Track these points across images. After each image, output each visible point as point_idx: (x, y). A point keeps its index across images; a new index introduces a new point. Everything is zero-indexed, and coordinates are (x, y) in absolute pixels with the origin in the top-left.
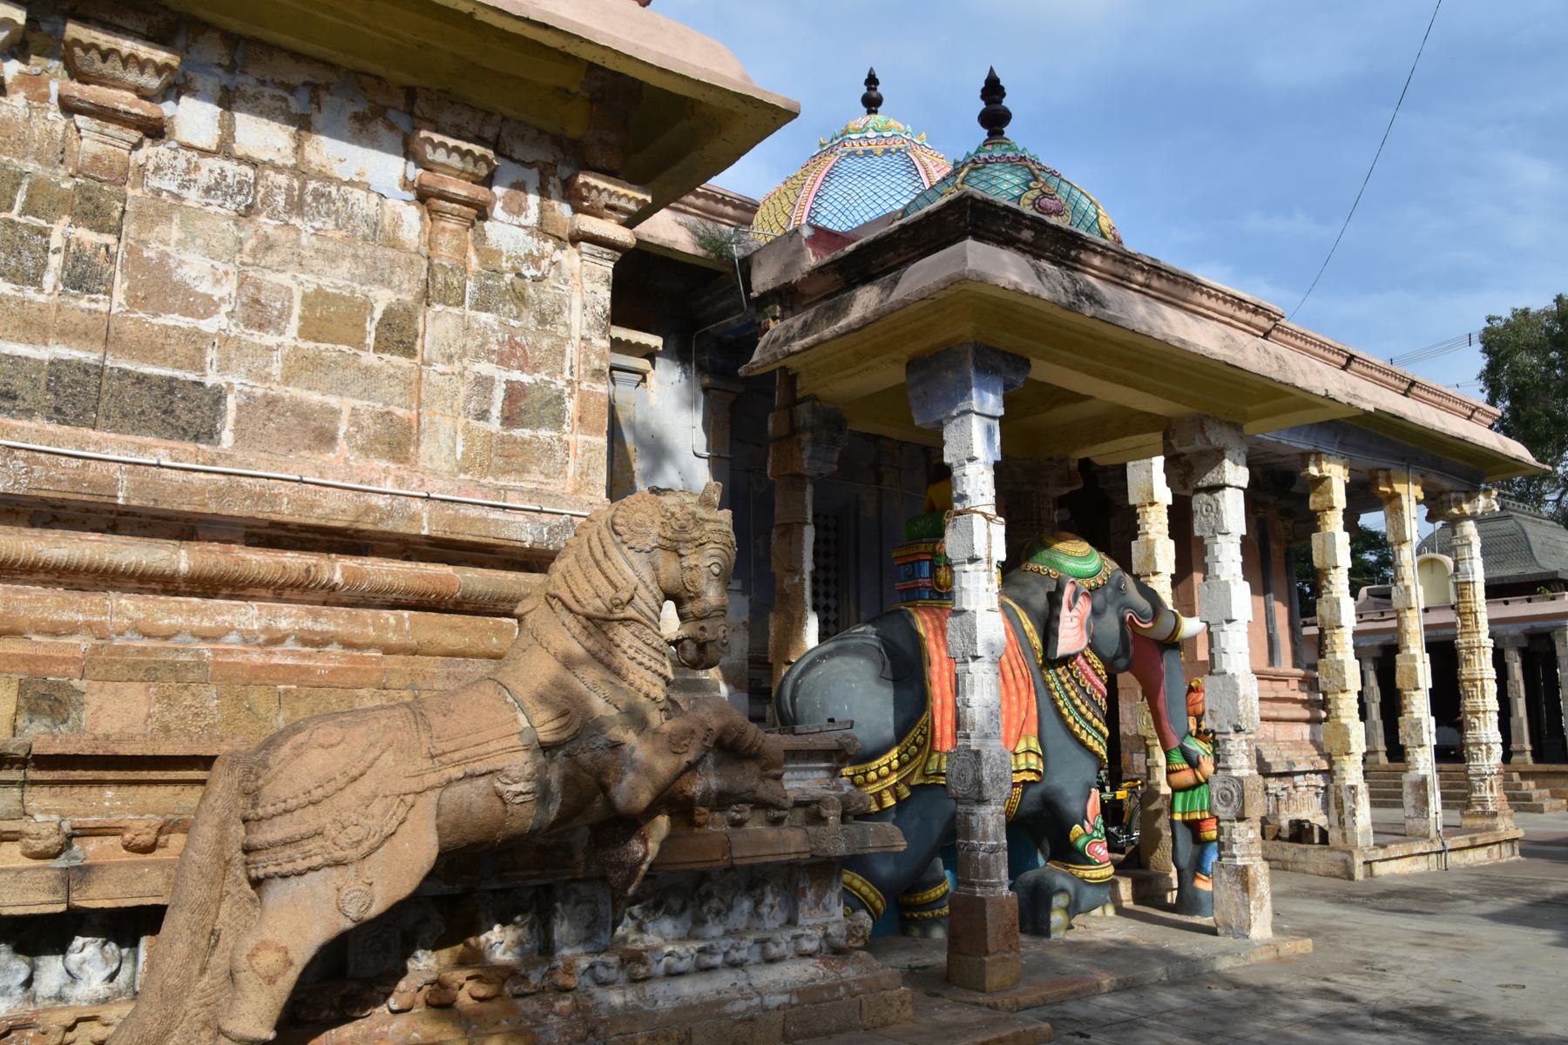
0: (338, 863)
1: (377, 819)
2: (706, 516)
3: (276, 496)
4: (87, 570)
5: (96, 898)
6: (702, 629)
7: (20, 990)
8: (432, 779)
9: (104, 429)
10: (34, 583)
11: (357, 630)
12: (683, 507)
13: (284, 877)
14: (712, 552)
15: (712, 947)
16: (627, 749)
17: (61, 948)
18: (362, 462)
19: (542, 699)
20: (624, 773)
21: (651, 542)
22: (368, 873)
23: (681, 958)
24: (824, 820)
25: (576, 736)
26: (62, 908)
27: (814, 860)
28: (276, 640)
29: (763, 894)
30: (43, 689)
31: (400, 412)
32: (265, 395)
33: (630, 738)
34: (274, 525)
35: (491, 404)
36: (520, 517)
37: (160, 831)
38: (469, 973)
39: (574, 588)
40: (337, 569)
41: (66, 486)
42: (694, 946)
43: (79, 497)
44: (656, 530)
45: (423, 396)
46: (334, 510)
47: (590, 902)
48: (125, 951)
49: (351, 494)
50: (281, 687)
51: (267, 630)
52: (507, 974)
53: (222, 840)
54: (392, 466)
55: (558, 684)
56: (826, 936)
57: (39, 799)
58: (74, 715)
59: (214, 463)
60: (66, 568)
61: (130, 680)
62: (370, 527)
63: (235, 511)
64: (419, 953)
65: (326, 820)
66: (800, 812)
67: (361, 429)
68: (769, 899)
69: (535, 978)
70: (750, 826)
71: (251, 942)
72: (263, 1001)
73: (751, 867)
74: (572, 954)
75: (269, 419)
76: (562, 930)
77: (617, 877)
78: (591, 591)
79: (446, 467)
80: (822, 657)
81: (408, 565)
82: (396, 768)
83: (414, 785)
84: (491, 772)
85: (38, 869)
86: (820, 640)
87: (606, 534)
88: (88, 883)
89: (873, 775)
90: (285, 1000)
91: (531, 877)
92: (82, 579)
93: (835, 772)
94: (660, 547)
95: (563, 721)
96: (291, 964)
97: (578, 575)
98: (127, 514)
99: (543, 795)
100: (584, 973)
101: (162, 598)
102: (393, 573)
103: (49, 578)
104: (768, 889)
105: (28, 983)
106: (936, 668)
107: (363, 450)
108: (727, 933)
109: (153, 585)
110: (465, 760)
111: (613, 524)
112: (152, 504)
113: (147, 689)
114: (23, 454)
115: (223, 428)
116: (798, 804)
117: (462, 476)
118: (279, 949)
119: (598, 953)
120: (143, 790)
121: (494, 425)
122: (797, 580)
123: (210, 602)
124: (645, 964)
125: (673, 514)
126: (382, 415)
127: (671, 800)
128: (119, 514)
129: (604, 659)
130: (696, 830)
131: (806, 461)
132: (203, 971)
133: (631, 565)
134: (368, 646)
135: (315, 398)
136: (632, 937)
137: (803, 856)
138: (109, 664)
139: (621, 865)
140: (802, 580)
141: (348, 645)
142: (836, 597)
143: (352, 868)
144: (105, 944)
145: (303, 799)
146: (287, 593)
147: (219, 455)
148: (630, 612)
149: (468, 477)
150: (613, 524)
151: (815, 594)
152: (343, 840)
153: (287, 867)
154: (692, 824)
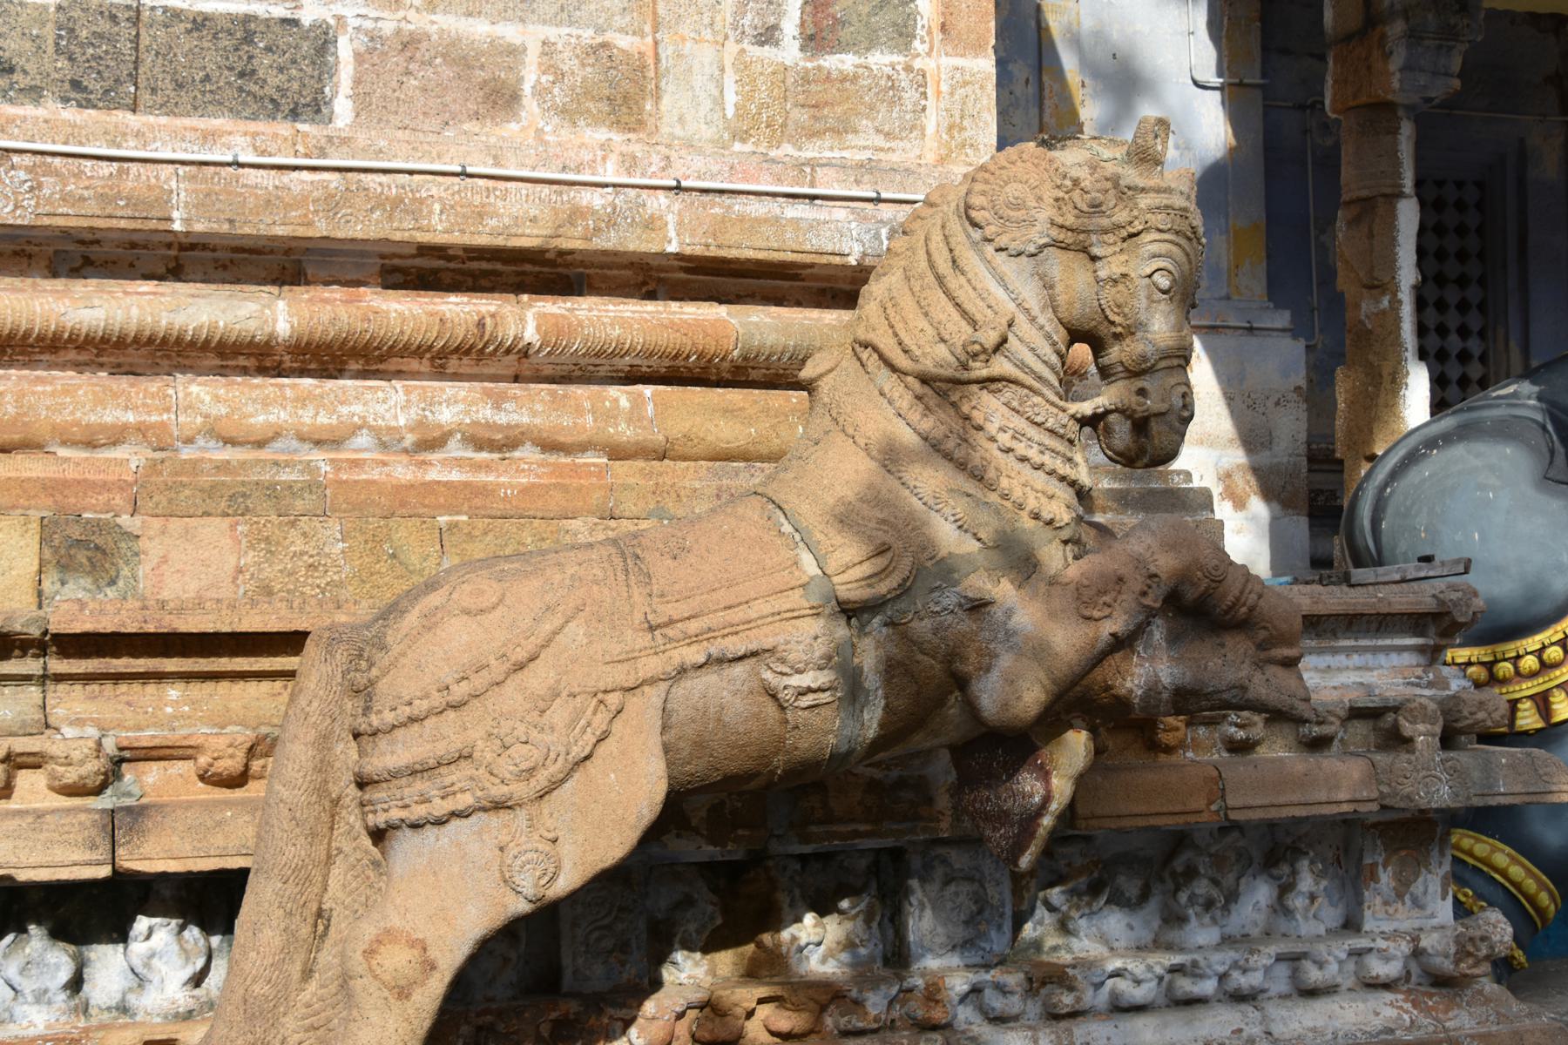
0: (498, 806)
1: (560, 733)
2: (1141, 183)
3: (422, 201)
4: (136, 340)
5: (153, 855)
6: (1142, 392)
7: (63, 996)
8: (651, 665)
9: (150, 109)
10: (63, 366)
11: (567, 421)
12: (1094, 168)
13: (415, 826)
14: (1155, 248)
15: (1195, 964)
16: (997, 612)
17: (119, 933)
18: (565, 134)
19: (845, 519)
20: (994, 656)
21: (1038, 234)
22: (549, 823)
23: (1138, 982)
24: (1406, 742)
25: (904, 590)
26: (104, 872)
27: (1389, 816)
28: (431, 442)
29: (1294, 873)
30: (76, 532)
31: (623, 42)
32: (398, 32)
33: (1003, 591)
34: (425, 250)
35: (780, 15)
36: (840, 213)
37: (251, 752)
38: (763, 991)
39: (899, 327)
40: (527, 319)
41: (92, 207)
42: (1162, 961)
43: (114, 223)
44: (1045, 213)
45: (661, 11)
46: (518, 220)
47: (970, 879)
48: (215, 940)
49: (546, 189)
50: (443, 520)
51: (420, 424)
52: (824, 997)
53: (323, 766)
54: (617, 137)
55: (873, 497)
56: (1417, 953)
57: (69, 703)
58: (125, 571)
59: (323, 154)
60: (105, 340)
61: (207, 514)
62: (577, 244)
63: (357, 231)
64: (679, 956)
65: (476, 734)
66: (1360, 729)
67: (560, 76)
68: (1306, 882)
69: (875, 1003)
70: (1262, 752)
71: (368, 930)
72: (391, 1025)
73: (1272, 825)
74: (943, 968)
75: (408, 73)
76: (921, 923)
77: (999, 836)
78: (930, 331)
79: (708, 133)
80: (1431, 443)
81: (650, 307)
82: (588, 651)
83: (620, 675)
84: (754, 654)
85: (68, 811)
86: (1432, 414)
87: (956, 227)
88: (142, 833)
89: (1530, 662)
90: (427, 1024)
91: (857, 834)
92: (133, 356)
93: (1433, 655)
94: (1056, 244)
95: (881, 562)
96: (433, 968)
97: (907, 303)
98: (193, 247)
99: (852, 689)
100: (963, 999)
101: (257, 381)
102: (623, 322)
103: (84, 357)
104: (1304, 865)
105: (76, 984)
106: (611, 307)
107: (568, 114)
108: (1227, 941)
109: (242, 361)
110: (708, 634)
111: (968, 207)
112: (225, 228)
113: (233, 527)
114: (28, 160)
115: (335, 94)
116: (1357, 713)
117: (737, 146)
118: (412, 944)
119: (987, 967)
120: (224, 685)
121: (789, 51)
122: (1385, 303)
123: (330, 384)
124: (1071, 989)
125: (1076, 182)
126: (595, 50)
127: (1079, 700)
128: (183, 248)
129: (956, 452)
130: (1163, 757)
131: (1395, 76)
132: (307, 974)
133: (1002, 281)
134: (583, 448)
135: (479, 29)
136: (1050, 942)
137: (1363, 808)
138: (177, 491)
139: (1003, 817)
140: (1396, 303)
141: (550, 446)
142: (1482, 334)
143: (522, 814)
144: (182, 928)
145: (437, 700)
146: (453, 364)
147: (330, 139)
148: (1000, 366)
149: (748, 147)
150: (968, 207)
151: (1421, 330)
152: (505, 767)
153: (419, 812)
154: (1155, 747)
